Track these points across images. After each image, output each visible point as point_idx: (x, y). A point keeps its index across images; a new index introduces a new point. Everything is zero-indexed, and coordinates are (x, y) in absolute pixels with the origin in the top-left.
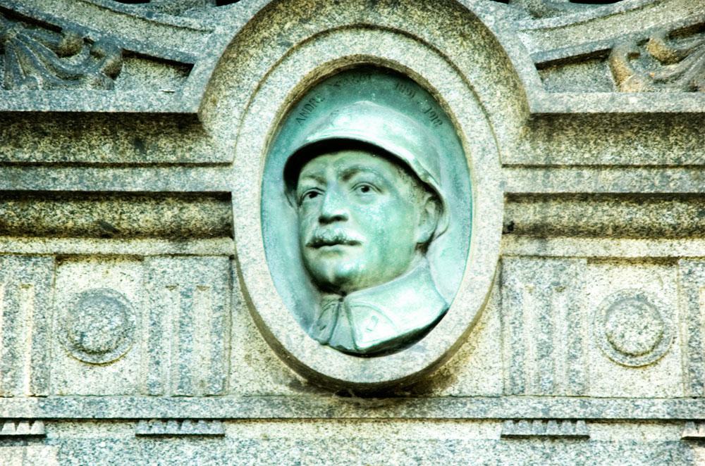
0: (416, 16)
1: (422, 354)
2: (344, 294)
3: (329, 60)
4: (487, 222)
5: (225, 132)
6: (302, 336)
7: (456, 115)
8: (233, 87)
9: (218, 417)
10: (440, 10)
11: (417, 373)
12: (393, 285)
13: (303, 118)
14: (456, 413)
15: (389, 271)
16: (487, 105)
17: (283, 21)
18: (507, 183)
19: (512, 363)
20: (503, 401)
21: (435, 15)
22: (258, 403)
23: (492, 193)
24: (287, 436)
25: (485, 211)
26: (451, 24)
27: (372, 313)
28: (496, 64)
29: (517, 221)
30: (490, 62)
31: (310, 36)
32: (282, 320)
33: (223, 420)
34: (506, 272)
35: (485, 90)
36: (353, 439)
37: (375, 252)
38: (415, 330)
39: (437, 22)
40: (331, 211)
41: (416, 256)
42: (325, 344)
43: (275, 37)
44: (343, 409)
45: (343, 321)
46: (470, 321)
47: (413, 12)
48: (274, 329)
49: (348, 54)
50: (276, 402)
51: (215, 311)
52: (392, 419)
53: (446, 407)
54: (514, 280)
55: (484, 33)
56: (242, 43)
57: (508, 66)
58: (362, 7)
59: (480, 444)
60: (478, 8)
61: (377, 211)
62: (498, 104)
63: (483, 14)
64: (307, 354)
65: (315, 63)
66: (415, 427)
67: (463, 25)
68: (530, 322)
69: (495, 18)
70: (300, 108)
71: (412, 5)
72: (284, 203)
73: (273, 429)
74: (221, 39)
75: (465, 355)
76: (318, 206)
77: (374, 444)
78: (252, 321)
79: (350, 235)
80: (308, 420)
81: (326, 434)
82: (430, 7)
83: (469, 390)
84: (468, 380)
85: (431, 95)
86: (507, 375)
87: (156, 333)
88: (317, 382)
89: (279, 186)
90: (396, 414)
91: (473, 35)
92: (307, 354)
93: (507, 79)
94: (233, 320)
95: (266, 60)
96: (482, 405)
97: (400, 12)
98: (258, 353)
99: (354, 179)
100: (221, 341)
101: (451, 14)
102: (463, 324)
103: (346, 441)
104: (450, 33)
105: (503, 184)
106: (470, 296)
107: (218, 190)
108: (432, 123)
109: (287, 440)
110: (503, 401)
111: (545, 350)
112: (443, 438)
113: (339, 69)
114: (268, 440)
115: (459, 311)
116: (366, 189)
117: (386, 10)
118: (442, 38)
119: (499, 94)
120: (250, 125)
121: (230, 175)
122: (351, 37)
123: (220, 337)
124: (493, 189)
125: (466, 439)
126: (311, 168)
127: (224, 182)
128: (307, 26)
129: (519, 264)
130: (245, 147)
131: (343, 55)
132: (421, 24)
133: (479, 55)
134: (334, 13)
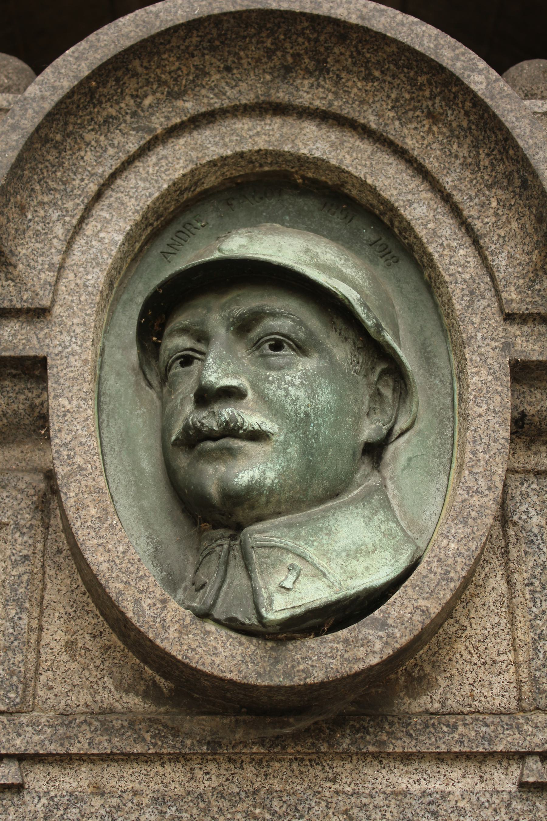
0: (355, 90)
1: (381, 633)
2: (239, 527)
3: (215, 157)
4: (485, 407)
5: (40, 260)
6: (164, 601)
7: (425, 241)
8: (55, 190)
9: (12, 751)
10: (394, 76)
11: (371, 668)
12: (328, 510)
13: (171, 250)
14: (440, 743)
15: (317, 489)
16: (476, 222)
17: (141, 92)
18: (514, 345)
19: (531, 653)
20: (521, 721)
21: (386, 87)
22: (84, 727)
23: (489, 361)
24: (137, 786)
25: (481, 390)
26: (412, 99)
27: (290, 559)
28: (488, 155)
29: (530, 410)
30: (478, 154)
31: (185, 118)
32: (127, 572)
33: (20, 758)
34: (513, 498)
35: (471, 199)
36: (256, 792)
37: (294, 450)
38: (365, 589)
39: (388, 97)
40: (216, 376)
41: (363, 467)
42: (204, 615)
43: (128, 118)
44: (237, 736)
45: (237, 574)
46: (464, 574)
47: (350, 84)
48: (114, 587)
49: (246, 147)
50: (117, 724)
51: (15, 564)
52: (325, 753)
53: (420, 732)
54: (527, 512)
55: (468, 104)
56: (72, 119)
57: (511, 152)
58: (268, 77)
59: (483, 799)
60: (459, 64)
61: (297, 381)
62: (494, 219)
63: (467, 73)
64: (172, 633)
65: (192, 161)
66: (365, 770)
67: (432, 97)
69: (487, 78)
70: (168, 237)
71: (349, 72)
72: (137, 384)
73: (113, 777)
74: (35, 105)
75: (450, 641)
77: (293, 800)
78: (80, 582)
79: (252, 418)
80: (175, 758)
81: (207, 783)
82: (377, 74)
83: (458, 702)
84: (456, 685)
86: (524, 674)
88: (184, 691)
89: (126, 353)
90: (331, 746)
91: (450, 112)
92: (172, 633)
93: (509, 177)
94: (48, 580)
95: (111, 151)
96: (484, 729)
97: (328, 84)
98: (88, 637)
99: (257, 331)
100: (24, 616)
101: (412, 82)
102: (452, 579)
103: (243, 795)
104: (410, 114)
105: (507, 346)
106: (462, 531)
107: (24, 354)
108: (382, 261)
109: (135, 793)
110: (521, 721)
112: (415, 789)
113: (232, 180)
114: (102, 794)
115: (442, 556)
116: (277, 346)
117: (306, 82)
118: (397, 123)
119: (494, 204)
120: (83, 253)
121: (46, 330)
122: (250, 124)
123: (22, 609)
124: (491, 354)
125: (457, 790)
126: (183, 319)
127: (35, 341)
128: (179, 103)
129: (534, 486)
130: (73, 286)
131: (238, 149)
132: (362, 102)
133: (460, 145)
134: (223, 84)
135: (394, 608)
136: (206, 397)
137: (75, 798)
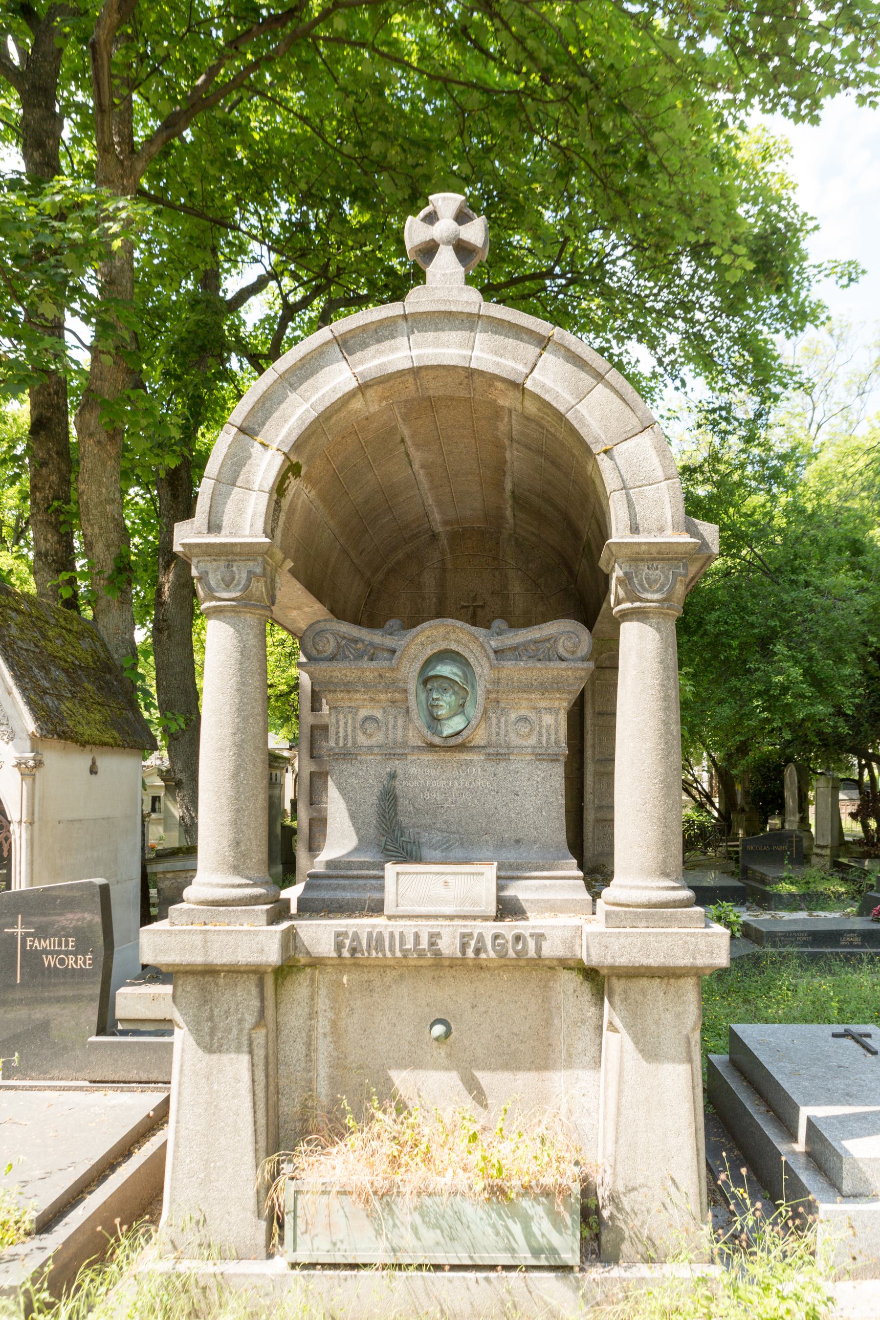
73: (422, 757)
76: (396, 765)
85: (458, 653)
111: (498, 734)
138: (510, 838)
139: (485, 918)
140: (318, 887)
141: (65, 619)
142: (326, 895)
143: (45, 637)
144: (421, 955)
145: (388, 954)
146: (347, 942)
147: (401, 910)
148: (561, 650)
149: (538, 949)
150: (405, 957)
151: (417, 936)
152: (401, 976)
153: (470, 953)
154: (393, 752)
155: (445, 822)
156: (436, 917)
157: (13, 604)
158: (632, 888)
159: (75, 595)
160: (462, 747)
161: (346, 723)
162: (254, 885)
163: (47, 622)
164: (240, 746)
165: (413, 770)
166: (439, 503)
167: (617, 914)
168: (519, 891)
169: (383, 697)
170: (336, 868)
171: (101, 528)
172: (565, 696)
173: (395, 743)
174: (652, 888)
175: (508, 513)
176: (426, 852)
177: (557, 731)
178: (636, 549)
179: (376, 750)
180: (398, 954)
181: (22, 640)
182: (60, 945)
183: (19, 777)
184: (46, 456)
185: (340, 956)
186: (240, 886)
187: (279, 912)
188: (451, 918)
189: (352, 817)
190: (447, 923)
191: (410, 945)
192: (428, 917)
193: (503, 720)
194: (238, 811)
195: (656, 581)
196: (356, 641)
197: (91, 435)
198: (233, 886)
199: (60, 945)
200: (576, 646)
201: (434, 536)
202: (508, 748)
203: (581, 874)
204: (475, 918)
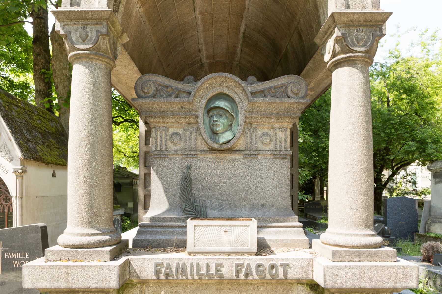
40: (215, 119)
68: (249, 138)
73: (207, 156)
79: (218, 123)
85: (228, 95)
87: (186, 140)
111: (251, 143)
135: (232, 141)
136: (214, 121)
137: (202, 158)
138: (258, 203)
139: (250, 254)
140: (145, 233)
141: (43, 113)
142: (150, 237)
143: (31, 118)
144: (211, 277)
145: (190, 277)
146: (163, 270)
147: (197, 249)
148: (290, 93)
149: (285, 273)
150: (200, 278)
151: (208, 266)
152: (197, 289)
153: (242, 276)
154: (189, 153)
155: (220, 194)
156: (219, 253)
157: (15, 102)
158: (346, 235)
159: (51, 106)
160: (230, 151)
161: (161, 137)
162: (103, 234)
163: (33, 113)
164: (92, 145)
165: (201, 164)
166: (206, 43)
167: (340, 253)
168: (269, 235)
169: (183, 120)
170: (156, 221)
171: (61, 80)
172: (291, 120)
173: (191, 148)
174: (360, 235)
175: (239, 50)
176: (210, 212)
177: (286, 141)
178: (351, 17)
179: (179, 152)
180: (196, 277)
181: (18, 118)
182: (21, 256)
183: (15, 177)
184: (39, 52)
185: (158, 278)
186: (93, 235)
187: (120, 249)
188: (229, 253)
189: (166, 191)
190: (226, 257)
191: (203, 271)
192: (214, 253)
193: (254, 135)
194: (91, 186)
195: (362, 39)
196: (167, 87)
197: (56, 41)
198: (88, 235)
199: (21, 256)
200: (299, 90)
201: (202, 65)
202: (257, 151)
203: (301, 224)
204: (244, 253)
